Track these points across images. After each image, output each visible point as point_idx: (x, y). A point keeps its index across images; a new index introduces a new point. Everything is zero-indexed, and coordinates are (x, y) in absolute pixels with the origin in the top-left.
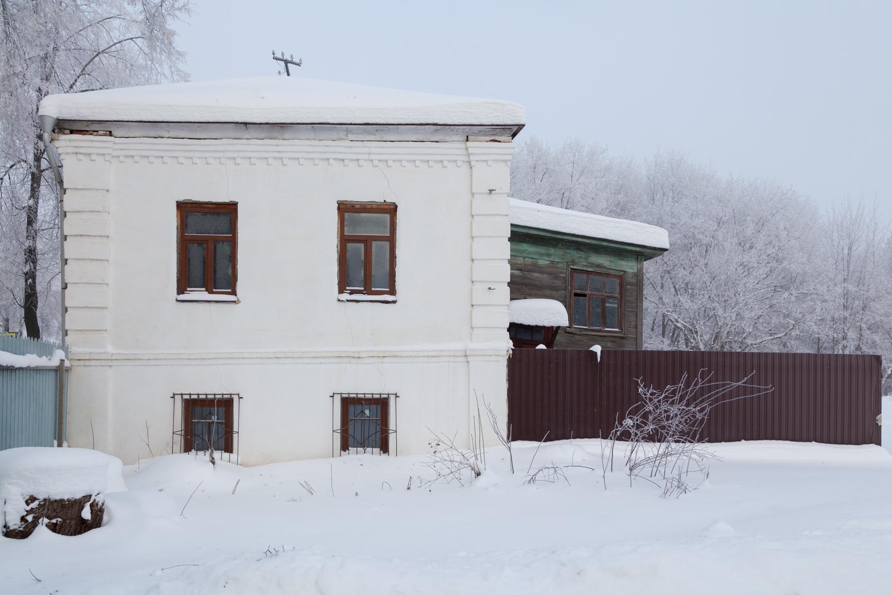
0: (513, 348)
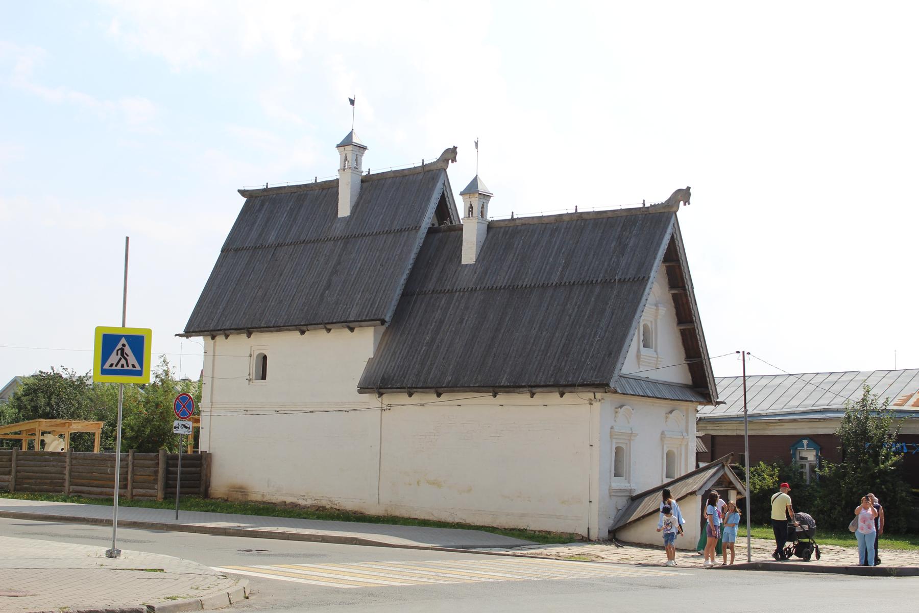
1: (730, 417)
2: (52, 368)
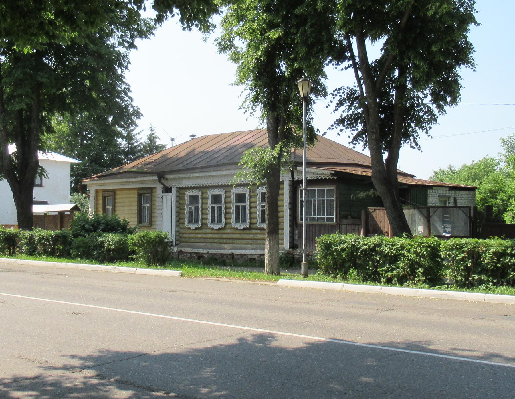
2: (152, 3)
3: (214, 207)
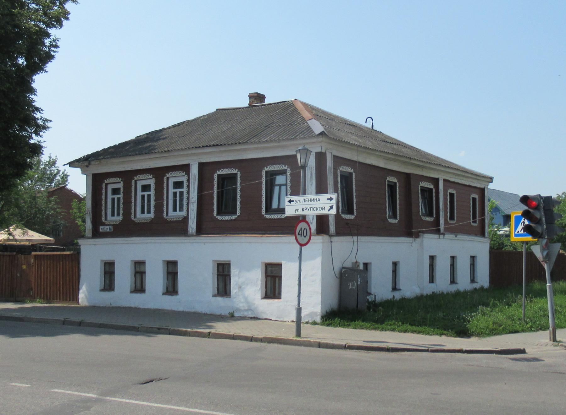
0: (33, 97)
1: (472, 275)
2: (44, 132)
3: (180, 211)
